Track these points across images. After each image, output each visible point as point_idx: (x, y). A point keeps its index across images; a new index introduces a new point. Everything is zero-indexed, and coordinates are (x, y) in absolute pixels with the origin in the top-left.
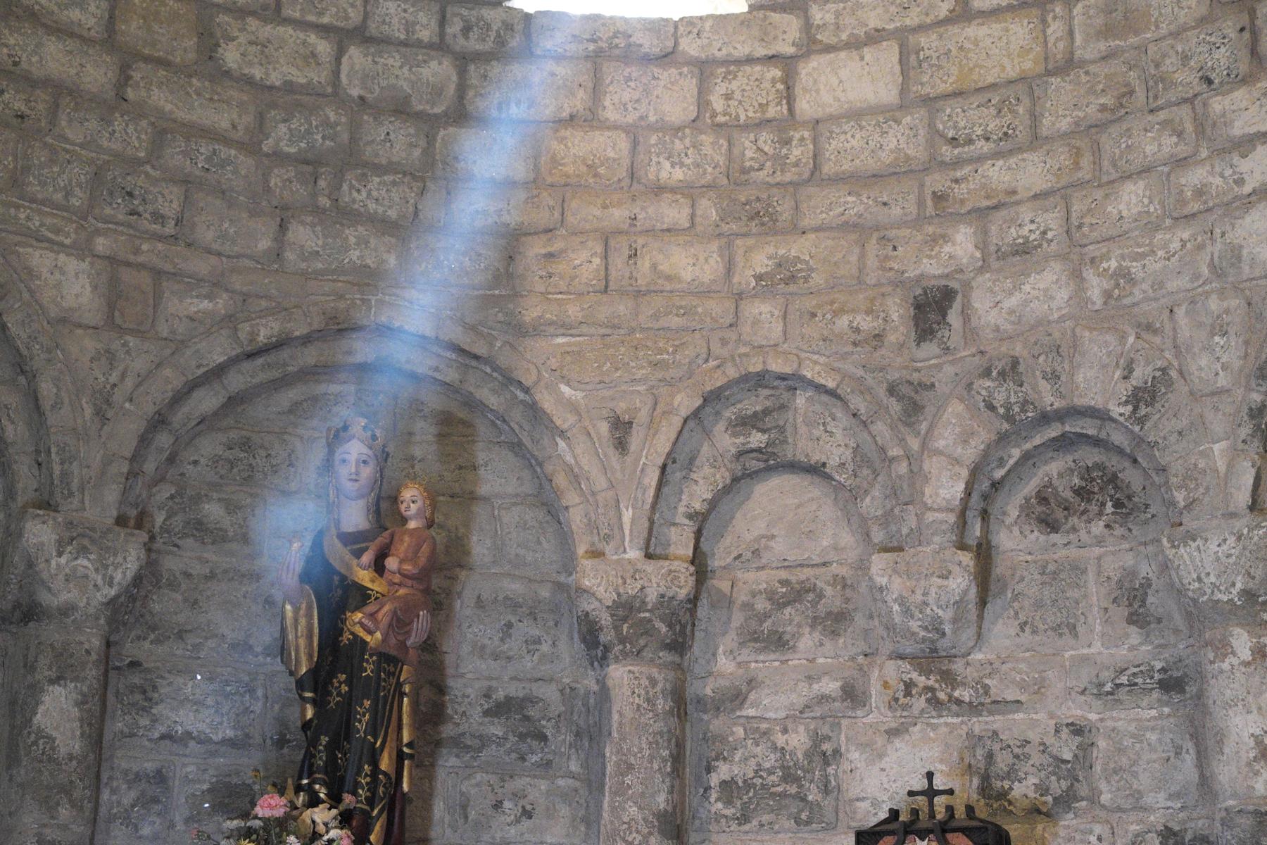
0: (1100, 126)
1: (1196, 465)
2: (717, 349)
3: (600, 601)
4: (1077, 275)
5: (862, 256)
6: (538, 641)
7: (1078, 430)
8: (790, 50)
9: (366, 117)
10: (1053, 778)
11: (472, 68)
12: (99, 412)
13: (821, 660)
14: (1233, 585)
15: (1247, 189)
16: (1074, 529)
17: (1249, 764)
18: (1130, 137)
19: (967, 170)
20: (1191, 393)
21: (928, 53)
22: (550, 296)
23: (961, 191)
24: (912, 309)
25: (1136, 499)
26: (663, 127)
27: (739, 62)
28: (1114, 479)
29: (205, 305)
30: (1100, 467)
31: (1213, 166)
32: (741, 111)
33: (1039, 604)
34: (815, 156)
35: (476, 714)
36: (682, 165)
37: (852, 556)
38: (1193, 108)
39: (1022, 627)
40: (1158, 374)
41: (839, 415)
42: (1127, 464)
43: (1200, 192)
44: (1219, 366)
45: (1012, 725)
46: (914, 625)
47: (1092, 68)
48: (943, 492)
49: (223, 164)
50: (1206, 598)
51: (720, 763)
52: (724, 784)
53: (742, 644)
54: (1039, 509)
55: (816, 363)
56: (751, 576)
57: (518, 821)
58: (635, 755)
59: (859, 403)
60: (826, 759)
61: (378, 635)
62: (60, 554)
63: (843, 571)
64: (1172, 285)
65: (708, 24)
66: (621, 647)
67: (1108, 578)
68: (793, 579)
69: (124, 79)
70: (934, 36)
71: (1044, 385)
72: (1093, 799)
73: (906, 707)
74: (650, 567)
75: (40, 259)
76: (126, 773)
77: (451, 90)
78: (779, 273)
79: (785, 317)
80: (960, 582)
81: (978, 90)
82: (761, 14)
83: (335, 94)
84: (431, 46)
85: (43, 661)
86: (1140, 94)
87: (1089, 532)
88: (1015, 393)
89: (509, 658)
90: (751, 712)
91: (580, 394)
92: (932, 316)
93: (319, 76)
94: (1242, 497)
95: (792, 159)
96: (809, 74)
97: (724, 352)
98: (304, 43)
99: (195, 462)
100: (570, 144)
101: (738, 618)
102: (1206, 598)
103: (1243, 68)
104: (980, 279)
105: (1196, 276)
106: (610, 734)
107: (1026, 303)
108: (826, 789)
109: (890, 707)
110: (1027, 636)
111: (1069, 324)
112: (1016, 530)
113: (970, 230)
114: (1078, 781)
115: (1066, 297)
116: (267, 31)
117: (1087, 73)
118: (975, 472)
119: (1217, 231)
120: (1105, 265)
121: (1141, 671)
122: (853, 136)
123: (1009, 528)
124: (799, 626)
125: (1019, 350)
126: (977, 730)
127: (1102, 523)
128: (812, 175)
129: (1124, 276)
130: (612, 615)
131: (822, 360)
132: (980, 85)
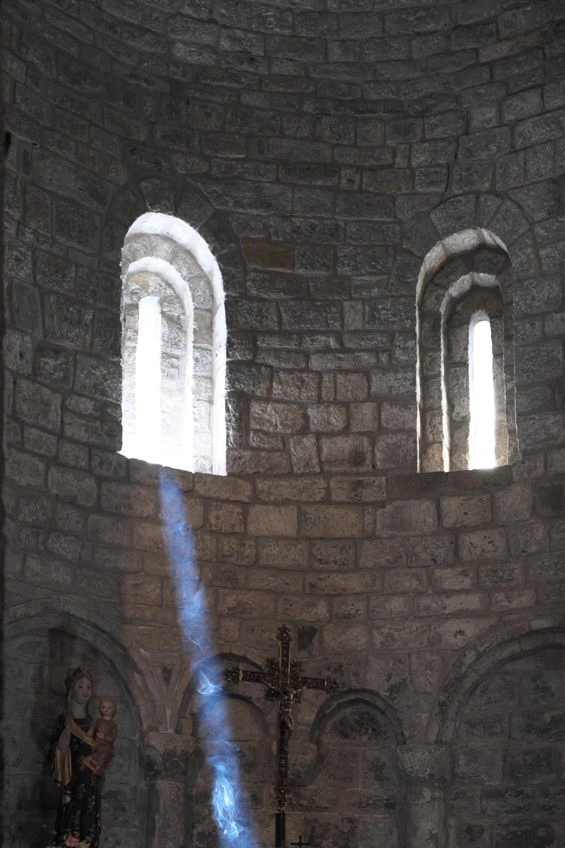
1: (414, 721)
3: (158, 751)
4: (370, 632)
6: (122, 766)
7: (363, 698)
8: (246, 500)
9: (59, 505)
10: (340, 839)
14: (426, 771)
15: (447, 612)
16: (354, 738)
17: (426, 840)
18: (398, 577)
19: (325, 575)
21: (311, 516)
22: (137, 605)
24: (297, 635)
25: (382, 729)
27: (223, 501)
28: (373, 719)
31: (434, 598)
32: (223, 526)
34: (256, 555)
38: (427, 571)
40: (402, 681)
43: (427, 608)
44: (428, 682)
47: (385, 542)
48: (306, 718)
50: (414, 775)
51: (198, 825)
52: (199, 833)
55: (253, 652)
58: (171, 821)
61: (98, 768)
64: (411, 645)
66: (166, 773)
67: (368, 760)
70: (314, 509)
74: (178, 737)
78: (239, 608)
82: (233, 479)
87: (360, 740)
88: (340, 679)
91: (149, 654)
94: (432, 737)
96: (255, 514)
100: (147, 530)
102: (414, 775)
105: (422, 643)
106: (158, 810)
109: (272, 805)
111: (365, 653)
114: (349, 841)
115: (365, 641)
117: (382, 543)
118: (321, 710)
119: (432, 627)
120: (383, 630)
121: (378, 799)
122: (274, 549)
126: (308, 817)
127: (366, 737)
128: (254, 563)
129: (389, 636)
130: (163, 758)
131: (256, 651)
132: (334, 537)
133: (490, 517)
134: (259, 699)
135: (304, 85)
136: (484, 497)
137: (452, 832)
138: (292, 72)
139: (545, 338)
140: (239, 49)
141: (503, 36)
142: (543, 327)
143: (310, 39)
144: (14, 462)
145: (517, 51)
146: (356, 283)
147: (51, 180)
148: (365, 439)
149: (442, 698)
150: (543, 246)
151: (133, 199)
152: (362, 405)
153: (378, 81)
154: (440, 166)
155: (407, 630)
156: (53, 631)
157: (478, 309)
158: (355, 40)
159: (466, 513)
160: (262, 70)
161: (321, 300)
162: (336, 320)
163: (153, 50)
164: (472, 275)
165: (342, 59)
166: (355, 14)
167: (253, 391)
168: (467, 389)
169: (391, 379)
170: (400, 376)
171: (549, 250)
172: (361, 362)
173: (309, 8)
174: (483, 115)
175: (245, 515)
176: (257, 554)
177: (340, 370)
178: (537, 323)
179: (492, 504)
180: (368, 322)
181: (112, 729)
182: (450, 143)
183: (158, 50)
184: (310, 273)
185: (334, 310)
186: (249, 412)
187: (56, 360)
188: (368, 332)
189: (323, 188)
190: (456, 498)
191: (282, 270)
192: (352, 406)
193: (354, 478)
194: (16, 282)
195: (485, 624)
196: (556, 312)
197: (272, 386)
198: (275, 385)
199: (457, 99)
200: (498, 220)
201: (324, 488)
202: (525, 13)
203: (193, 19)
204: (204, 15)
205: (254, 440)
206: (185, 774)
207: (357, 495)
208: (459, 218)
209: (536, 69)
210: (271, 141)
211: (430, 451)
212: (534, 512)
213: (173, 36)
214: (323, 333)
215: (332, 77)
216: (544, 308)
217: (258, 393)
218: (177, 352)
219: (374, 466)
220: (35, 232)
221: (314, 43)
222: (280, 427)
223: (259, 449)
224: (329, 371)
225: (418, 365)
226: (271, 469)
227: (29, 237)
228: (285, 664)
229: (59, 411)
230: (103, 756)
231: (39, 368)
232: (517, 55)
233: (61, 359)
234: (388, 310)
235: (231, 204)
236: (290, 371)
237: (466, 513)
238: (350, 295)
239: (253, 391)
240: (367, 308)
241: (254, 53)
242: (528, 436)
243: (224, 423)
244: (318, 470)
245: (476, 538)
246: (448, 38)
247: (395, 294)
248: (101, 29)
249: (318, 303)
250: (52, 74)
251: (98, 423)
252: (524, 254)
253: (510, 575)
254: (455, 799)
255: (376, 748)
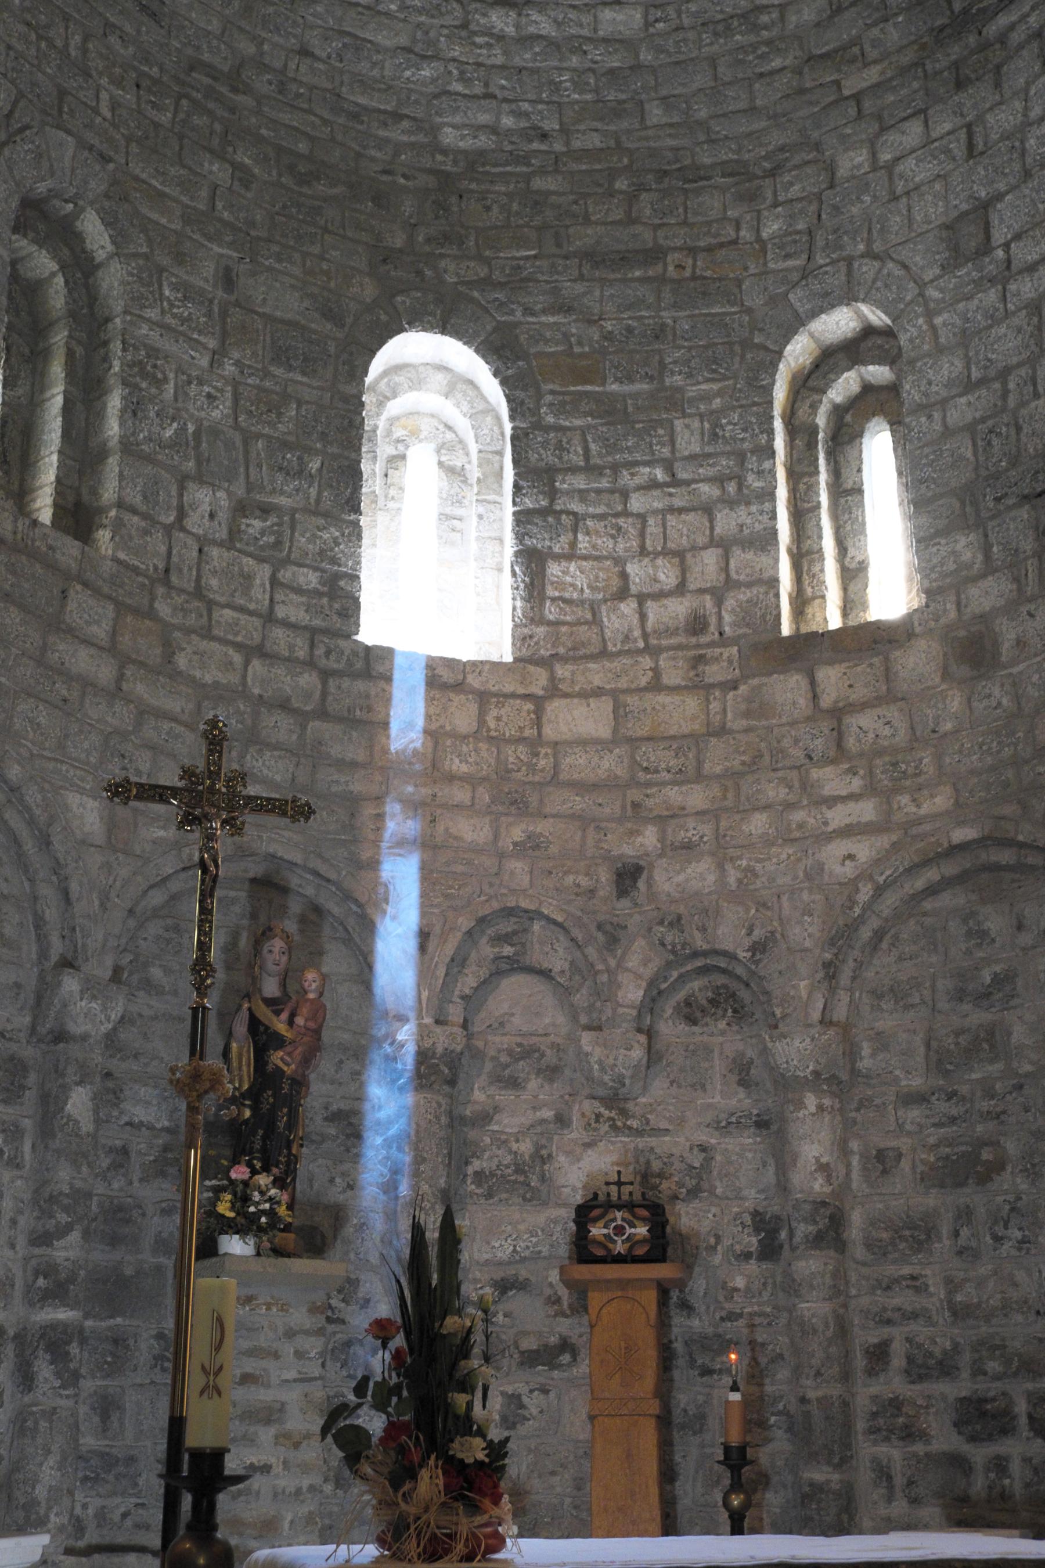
0: (741, 774)
2: (486, 888)
4: (721, 866)
5: (584, 838)
8: (541, 693)
11: (331, 681)
12: (102, 904)
13: (541, 1097)
15: (830, 829)
16: (707, 1024)
17: (811, 1173)
19: (654, 790)
20: (789, 949)
23: (650, 803)
26: (454, 735)
27: (506, 696)
29: (162, 833)
30: (725, 986)
33: (682, 1070)
34: (554, 767)
35: (319, 1119)
36: (467, 762)
37: (564, 1031)
39: (672, 1083)
41: (562, 938)
42: (742, 986)
43: (801, 826)
45: (663, 1144)
46: (606, 1078)
47: (737, 736)
49: (177, 737)
52: (476, 1173)
53: (491, 1083)
54: (687, 1010)
56: (497, 1039)
57: (344, 1191)
59: (578, 934)
60: (544, 1161)
62: (81, 999)
63: (559, 1040)
65: (487, 667)
68: (525, 1043)
69: (121, 677)
71: (698, 935)
72: (712, 1192)
73: (595, 1130)
74: (438, 1030)
75: (73, 799)
76: (104, 1146)
77: (317, 694)
79: (531, 872)
80: (638, 1053)
81: (665, 738)
82: (521, 665)
83: (244, 691)
84: (304, 663)
85: (70, 1070)
86: (767, 758)
89: (340, 1084)
90: (496, 1128)
92: (627, 882)
93: (234, 678)
94: (816, 1015)
95: (540, 766)
97: (491, 891)
98: (226, 654)
99: (145, 939)
101: (488, 1066)
103: (832, 754)
104: (659, 862)
105: (795, 878)
107: (687, 880)
108: (543, 1179)
110: (674, 1090)
111: (715, 897)
112: (670, 1022)
113: (655, 829)
116: (204, 645)
118: (652, 983)
119: (810, 852)
123: (666, 1021)
124: (528, 1073)
125: (682, 909)
126: (640, 1146)
129: (750, 870)
133: (884, 688)
134: (563, 972)
135: (615, 159)
136: (875, 660)
137: (855, 1161)
138: (598, 145)
139: (948, 432)
140: (527, 125)
141: (870, 59)
142: (944, 417)
143: (620, 102)
144: (195, 653)
145: (889, 74)
146: (691, 394)
147: (264, 299)
148: (708, 597)
149: (828, 956)
150: (939, 313)
151: (384, 317)
152: (702, 553)
153: (713, 141)
154: (798, 232)
155: (774, 860)
156: (253, 881)
157: (874, 415)
158: (680, 96)
159: (850, 686)
160: (558, 147)
161: (643, 422)
162: (663, 445)
163: (413, 139)
164: (858, 371)
165: (664, 120)
166: (677, 63)
167: (550, 548)
168: (864, 524)
169: (741, 514)
170: (754, 508)
171: (946, 315)
172: (700, 496)
173: (615, 64)
174: (852, 160)
175: (539, 712)
176: (556, 766)
177: (672, 510)
178: (936, 415)
179: (887, 670)
180: (709, 443)
181: (318, 1011)
182: (810, 202)
183: (421, 138)
184: (627, 388)
185: (661, 432)
186: (544, 576)
187: (266, 520)
188: (709, 455)
189: (641, 280)
190: (837, 666)
191: (588, 388)
192: (689, 556)
193: (693, 653)
194: (206, 423)
195: (884, 841)
196: (961, 395)
197: (576, 537)
198: (580, 537)
199: (817, 146)
200: (878, 289)
201: (651, 669)
202: (895, 25)
203: (465, 96)
204: (478, 89)
205: (551, 612)
206: (452, 1082)
207: (697, 675)
208: (827, 294)
209: (915, 92)
210: (571, 230)
211: (809, 611)
212: (946, 674)
213: (439, 120)
214: (647, 464)
215: (652, 144)
216: (944, 393)
217: (557, 549)
218: (459, 512)
219: (721, 634)
220: (237, 363)
221: (626, 106)
222: (587, 591)
223: (558, 623)
224: (655, 512)
225: (782, 493)
226: (574, 649)
227: (229, 369)
228: (214, 775)
229: (268, 586)
230: (300, 1049)
231: (239, 531)
232: (891, 79)
233: (272, 520)
234: (735, 424)
235: (518, 314)
236: (602, 517)
237: (850, 686)
238: (683, 411)
239: (550, 548)
240: (707, 425)
241: (547, 128)
242: (932, 569)
243: (510, 592)
244: (641, 644)
245: (866, 720)
246: (800, 73)
247: (744, 402)
248: (341, 120)
249: (639, 426)
250: (270, 175)
251: (325, 601)
252: (914, 326)
253: (916, 767)
254: (858, 1110)
255: (739, 1037)
